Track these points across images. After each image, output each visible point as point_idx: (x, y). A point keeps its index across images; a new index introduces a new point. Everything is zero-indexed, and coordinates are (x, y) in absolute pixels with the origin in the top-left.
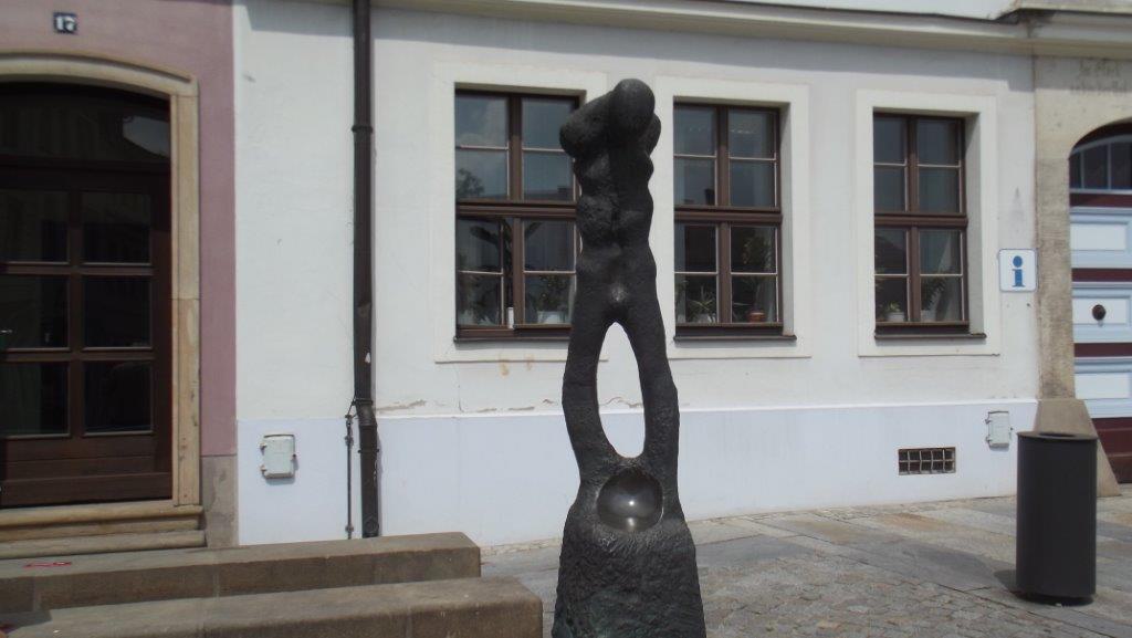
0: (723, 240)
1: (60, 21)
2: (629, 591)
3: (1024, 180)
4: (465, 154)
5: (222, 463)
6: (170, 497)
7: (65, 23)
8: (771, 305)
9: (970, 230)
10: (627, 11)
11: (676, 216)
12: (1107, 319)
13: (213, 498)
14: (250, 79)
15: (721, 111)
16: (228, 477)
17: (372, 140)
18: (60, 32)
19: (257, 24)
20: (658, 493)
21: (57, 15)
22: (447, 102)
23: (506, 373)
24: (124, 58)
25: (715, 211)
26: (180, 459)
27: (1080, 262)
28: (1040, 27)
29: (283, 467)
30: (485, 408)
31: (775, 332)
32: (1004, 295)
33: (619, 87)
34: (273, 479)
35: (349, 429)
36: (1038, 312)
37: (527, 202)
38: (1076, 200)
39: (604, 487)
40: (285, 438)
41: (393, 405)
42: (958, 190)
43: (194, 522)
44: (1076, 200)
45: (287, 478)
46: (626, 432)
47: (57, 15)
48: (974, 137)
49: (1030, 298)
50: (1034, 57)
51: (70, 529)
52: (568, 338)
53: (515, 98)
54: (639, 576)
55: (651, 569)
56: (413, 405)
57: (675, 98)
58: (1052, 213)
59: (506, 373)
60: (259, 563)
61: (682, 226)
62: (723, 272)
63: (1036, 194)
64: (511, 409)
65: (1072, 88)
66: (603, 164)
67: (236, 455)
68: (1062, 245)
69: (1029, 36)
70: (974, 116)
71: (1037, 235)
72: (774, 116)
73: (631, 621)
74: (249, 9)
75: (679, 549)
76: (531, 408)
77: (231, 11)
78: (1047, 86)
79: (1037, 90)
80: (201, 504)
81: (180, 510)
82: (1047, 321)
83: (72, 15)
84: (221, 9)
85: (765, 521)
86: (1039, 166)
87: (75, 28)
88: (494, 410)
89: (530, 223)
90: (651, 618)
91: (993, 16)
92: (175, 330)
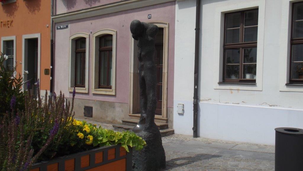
7: (149, 17)
12: (123, 27)
13: (170, 117)
19: (180, 8)
21: (148, 15)
23: (232, 93)
29: (181, 112)
30: (226, 102)
34: (180, 114)
37: (245, 43)
59: (232, 93)
64: (233, 103)
72: (84, 87)
76: (239, 104)
77: (175, 6)
83: (150, 15)
84: (173, 6)
88: (228, 103)
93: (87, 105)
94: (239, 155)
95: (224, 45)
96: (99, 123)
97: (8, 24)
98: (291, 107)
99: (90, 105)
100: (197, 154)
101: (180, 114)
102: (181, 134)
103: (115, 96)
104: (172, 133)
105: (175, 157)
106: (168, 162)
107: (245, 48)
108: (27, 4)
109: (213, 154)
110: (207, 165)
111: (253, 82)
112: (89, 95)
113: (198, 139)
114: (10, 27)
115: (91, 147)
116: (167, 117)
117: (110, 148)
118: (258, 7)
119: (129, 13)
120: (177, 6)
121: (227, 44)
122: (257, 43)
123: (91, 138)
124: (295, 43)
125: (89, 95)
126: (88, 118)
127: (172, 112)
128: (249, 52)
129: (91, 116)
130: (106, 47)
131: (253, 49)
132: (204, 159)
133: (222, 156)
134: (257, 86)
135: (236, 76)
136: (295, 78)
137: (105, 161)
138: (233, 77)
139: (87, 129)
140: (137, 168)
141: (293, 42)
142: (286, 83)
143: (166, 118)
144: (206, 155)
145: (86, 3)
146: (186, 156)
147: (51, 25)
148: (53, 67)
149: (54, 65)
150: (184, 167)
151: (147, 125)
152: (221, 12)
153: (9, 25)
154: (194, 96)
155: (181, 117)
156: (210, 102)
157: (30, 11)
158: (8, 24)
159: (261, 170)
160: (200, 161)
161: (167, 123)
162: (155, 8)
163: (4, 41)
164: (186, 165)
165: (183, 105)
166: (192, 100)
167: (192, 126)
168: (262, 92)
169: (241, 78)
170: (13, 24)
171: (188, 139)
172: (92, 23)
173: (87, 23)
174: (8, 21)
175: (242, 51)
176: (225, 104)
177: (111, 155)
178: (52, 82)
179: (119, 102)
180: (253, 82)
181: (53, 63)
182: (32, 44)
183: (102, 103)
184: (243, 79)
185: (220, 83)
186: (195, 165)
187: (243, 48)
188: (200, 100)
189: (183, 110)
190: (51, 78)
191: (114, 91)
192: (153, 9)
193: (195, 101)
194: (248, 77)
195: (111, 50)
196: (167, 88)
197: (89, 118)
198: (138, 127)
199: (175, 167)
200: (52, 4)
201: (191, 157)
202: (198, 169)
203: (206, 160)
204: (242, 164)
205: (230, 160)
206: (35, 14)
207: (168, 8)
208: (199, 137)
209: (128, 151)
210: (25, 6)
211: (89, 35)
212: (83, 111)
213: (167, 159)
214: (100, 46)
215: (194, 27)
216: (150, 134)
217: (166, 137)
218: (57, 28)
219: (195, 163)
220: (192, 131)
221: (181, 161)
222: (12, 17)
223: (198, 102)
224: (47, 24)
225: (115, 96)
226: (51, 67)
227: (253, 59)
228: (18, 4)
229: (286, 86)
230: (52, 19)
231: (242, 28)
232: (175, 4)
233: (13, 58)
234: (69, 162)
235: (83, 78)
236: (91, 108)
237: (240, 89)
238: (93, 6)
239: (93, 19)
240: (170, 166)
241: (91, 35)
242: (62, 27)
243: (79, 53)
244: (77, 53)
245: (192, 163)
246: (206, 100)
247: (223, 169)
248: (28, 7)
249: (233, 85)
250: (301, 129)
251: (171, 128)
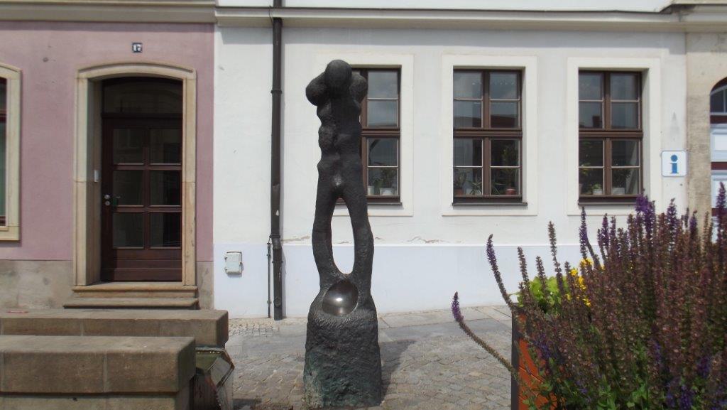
0: (607, 148)
1: (135, 47)
2: (331, 348)
3: (679, 108)
4: (457, 102)
5: (206, 265)
6: (181, 281)
8: (636, 182)
9: (644, 139)
10: (422, 20)
11: (580, 135)
14: (222, 69)
15: (606, 75)
16: (209, 272)
17: (282, 97)
18: (135, 52)
19: (226, 40)
20: (356, 294)
21: (134, 44)
22: (574, 78)
24: (161, 62)
25: (482, 130)
26: (186, 262)
27: (716, 158)
28: (687, 15)
29: (236, 269)
31: (517, 200)
32: (665, 179)
33: (329, 67)
34: (231, 274)
35: (269, 250)
36: (688, 189)
38: (715, 120)
39: (329, 290)
40: (235, 254)
41: (292, 238)
42: (638, 115)
43: (192, 294)
44: (715, 120)
45: (238, 274)
46: (344, 261)
47: (134, 44)
48: (647, 82)
49: (683, 181)
50: (686, 34)
51: (136, 294)
52: (635, 203)
53: (486, 73)
54: (336, 340)
55: (344, 337)
56: (303, 238)
57: (454, 67)
58: (698, 128)
60: (103, 320)
62: (607, 167)
63: (687, 117)
65: (712, 51)
66: (328, 108)
67: (212, 261)
68: (705, 148)
69: (680, 21)
70: (646, 70)
71: (688, 142)
73: (331, 365)
74: (222, 34)
75: (362, 327)
78: (696, 51)
79: (689, 54)
80: (196, 284)
81: (186, 288)
82: (693, 195)
83: (140, 44)
84: (208, 35)
85: (500, 310)
86: (689, 99)
87: (141, 50)
89: (373, 140)
90: (343, 364)
91: (658, 10)
92: (183, 197)
103: (17, 243)
120: (218, 36)
155: (235, 280)
161: (195, 297)
162: (155, 31)
194: (387, 193)
207: (195, 36)
208: (285, 317)
225: (17, 243)
232: (212, 31)
246: (298, 240)
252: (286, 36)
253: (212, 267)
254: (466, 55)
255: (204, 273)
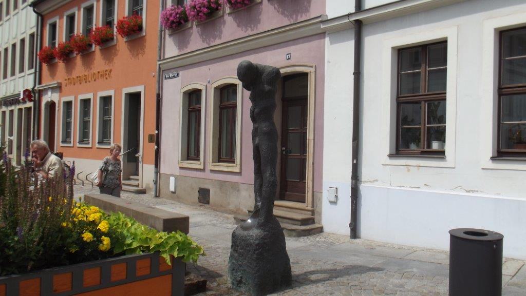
21: (287, 54)
29: (333, 199)
34: (331, 202)
56: (374, 181)
59: (409, 170)
61: (439, 114)
64: (410, 187)
72: (198, 160)
75: (251, 241)
76: (419, 187)
81: (306, 208)
84: (322, 40)
93: (202, 186)
94: (412, 269)
95: (398, 97)
96: (218, 213)
97: (106, 74)
98: (499, 194)
99: (206, 187)
100: (347, 265)
101: (331, 202)
102: (334, 233)
103: (240, 173)
104: (320, 230)
105: (312, 269)
106: (298, 276)
107: (430, 102)
108: (129, 47)
109: (371, 266)
110: (357, 283)
111: (441, 154)
112: (205, 172)
113: (357, 240)
114: (108, 78)
115: (110, 253)
116: (313, 206)
117: (140, 257)
118: (447, 38)
119: (260, 52)
120: (327, 40)
121: (403, 95)
122: (446, 93)
123: (106, 241)
124: (513, 92)
125: (205, 172)
126: (203, 204)
127: (320, 199)
128: (437, 106)
129: (208, 203)
130: (229, 103)
131: (442, 102)
132: (355, 273)
133: (385, 269)
134: (446, 161)
135: (418, 145)
136: (506, 149)
137: (131, 277)
138: (413, 147)
139: (103, 226)
140: (245, 284)
141: (502, 92)
142: (491, 155)
143: (310, 208)
144: (360, 266)
145: (203, 41)
146: (329, 267)
147: (157, 74)
148: (158, 131)
149: (161, 131)
150: (320, 285)
151: (262, 219)
152: (392, 48)
153: (107, 76)
154: (352, 176)
155: (333, 206)
156: (376, 185)
157: (133, 55)
158: (106, 74)
159: (439, 293)
160: (347, 276)
161: (313, 215)
162: (297, 44)
163: (81, 100)
164: (323, 282)
165: (337, 189)
166: (349, 182)
167: (348, 220)
168: (453, 169)
169: (424, 148)
170: (112, 72)
171: (342, 240)
172: (209, 69)
173: (204, 69)
174: (106, 71)
175: (424, 107)
176: (410, 189)
177: (143, 268)
178: (158, 153)
179: (246, 183)
180: (441, 154)
181: (158, 126)
182: (134, 99)
183: (222, 184)
184: (426, 149)
185: (391, 156)
186: (337, 282)
187: (425, 101)
188: (361, 182)
189: (336, 197)
190: (156, 147)
191: (238, 166)
192: (294, 45)
193: (353, 183)
194: (435, 146)
195: (234, 107)
196: (313, 164)
197: (205, 205)
198: (248, 222)
199: (307, 284)
200: (158, 44)
201: (335, 270)
202: (340, 289)
203: (357, 275)
204: (411, 284)
205: (395, 276)
206: (138, 59)
207: (315, 43)
208: (359, 238)
209: (170, 264)
210: (127, 49)
211: (206, 85)
212: (197, 194)
213: (292, 274)
214: (221, 102)
215: (352, 70)
216: (265, 233)
217: (309, 237)
218: (165, 78)
219: (338, 279)
220: (349, 229)
221: (318, 275)
222: (111, 65)
223: (358, 185)
224: (153, 72)
225: (240, 173)
226: (156, 132)
227: (442, 119)
228: (119, 47)
229: (491, 161)
230: (159, 65)
231: (423, 70)
232: (324, 38)
233: (110, 120)
234: (61, 278)
235: (232, 143)
236: (208, 191)
237: (421, 165)
238: (212, 44)
239: (211, 64)
240: (299, 282)
241: (208, 85)
242: (171, 76)
243: (193, 111)
244: (190, 112)
245: (335, 279)
246: (371, 182)
247: (379, 290)
248: (130, 51)
249: (419, 159)
250: (493, 232)
251: (319, 224)
252: (365, 31)
253: (322, 196)
254: (507, 15)
255: (318, 200)
